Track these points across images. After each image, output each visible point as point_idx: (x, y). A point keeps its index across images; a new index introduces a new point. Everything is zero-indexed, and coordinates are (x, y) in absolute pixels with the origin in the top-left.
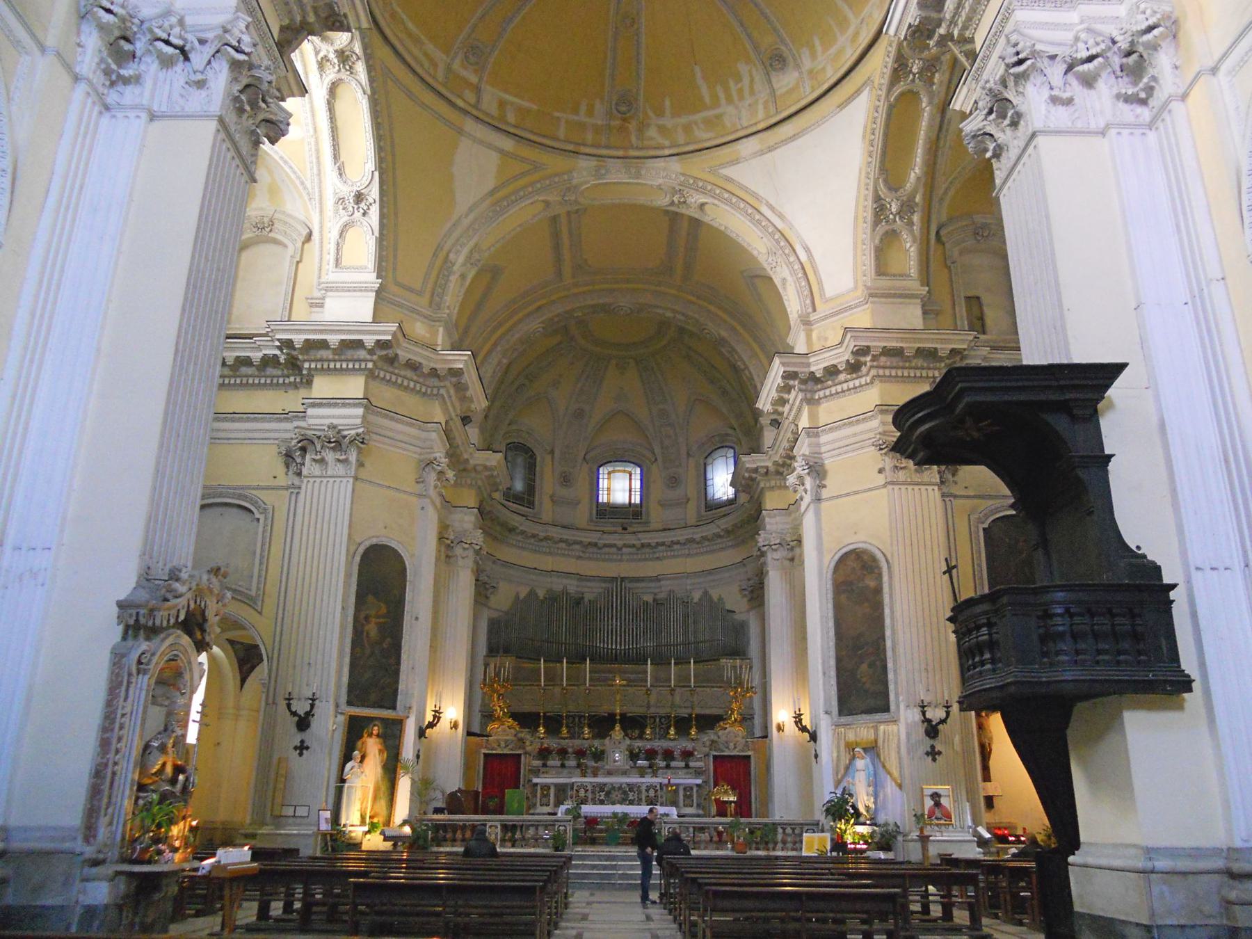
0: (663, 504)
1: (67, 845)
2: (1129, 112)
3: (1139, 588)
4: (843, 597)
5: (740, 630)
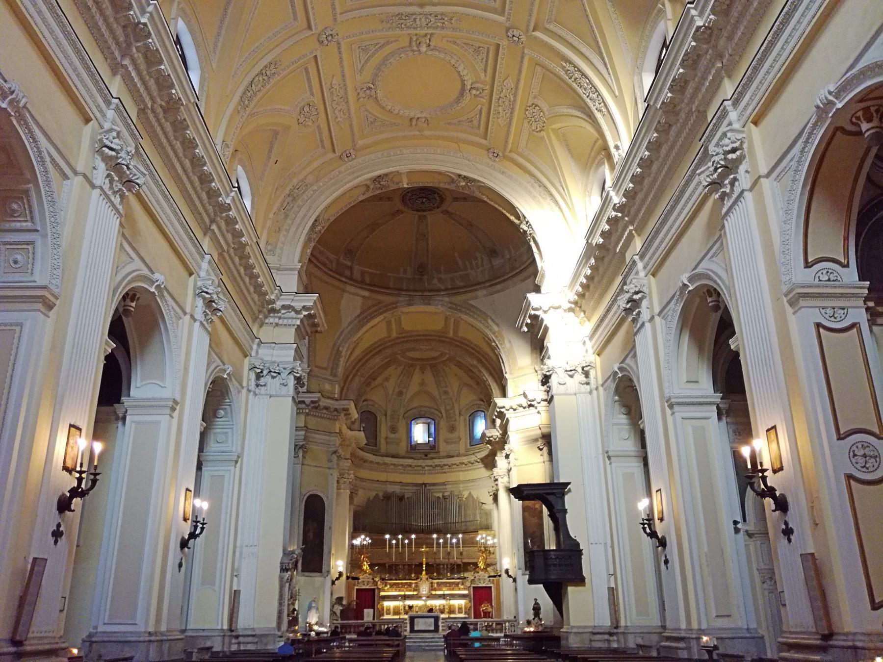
1: (272, 632)
3: (571, 551)
4: (526, 514)
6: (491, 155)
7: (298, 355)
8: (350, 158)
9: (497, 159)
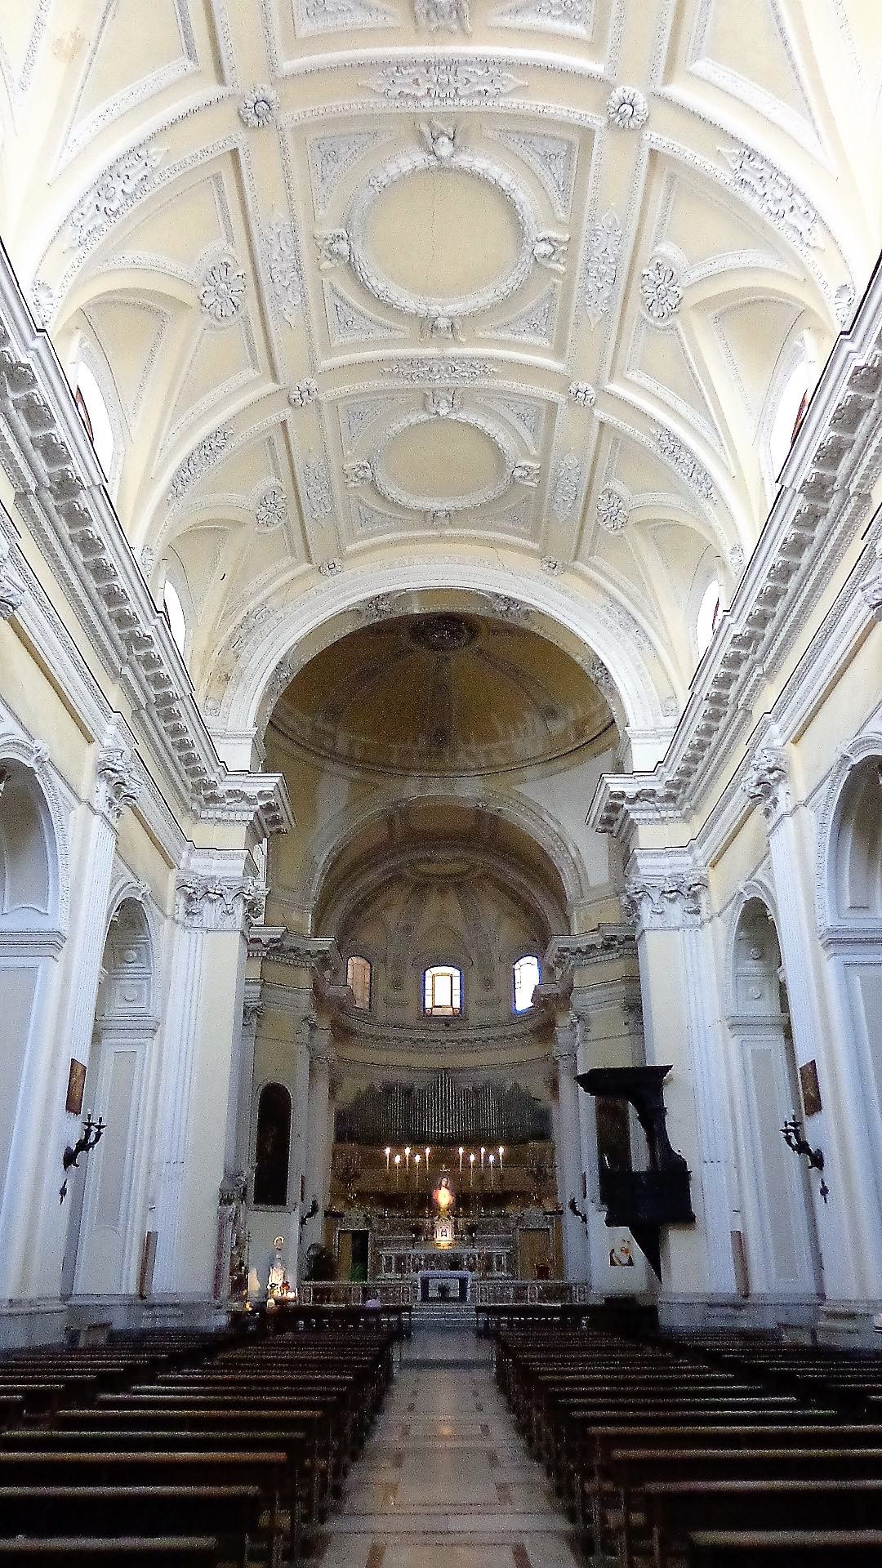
0: (481, 1003)
2: (691, 919)
5: (544, 1117)
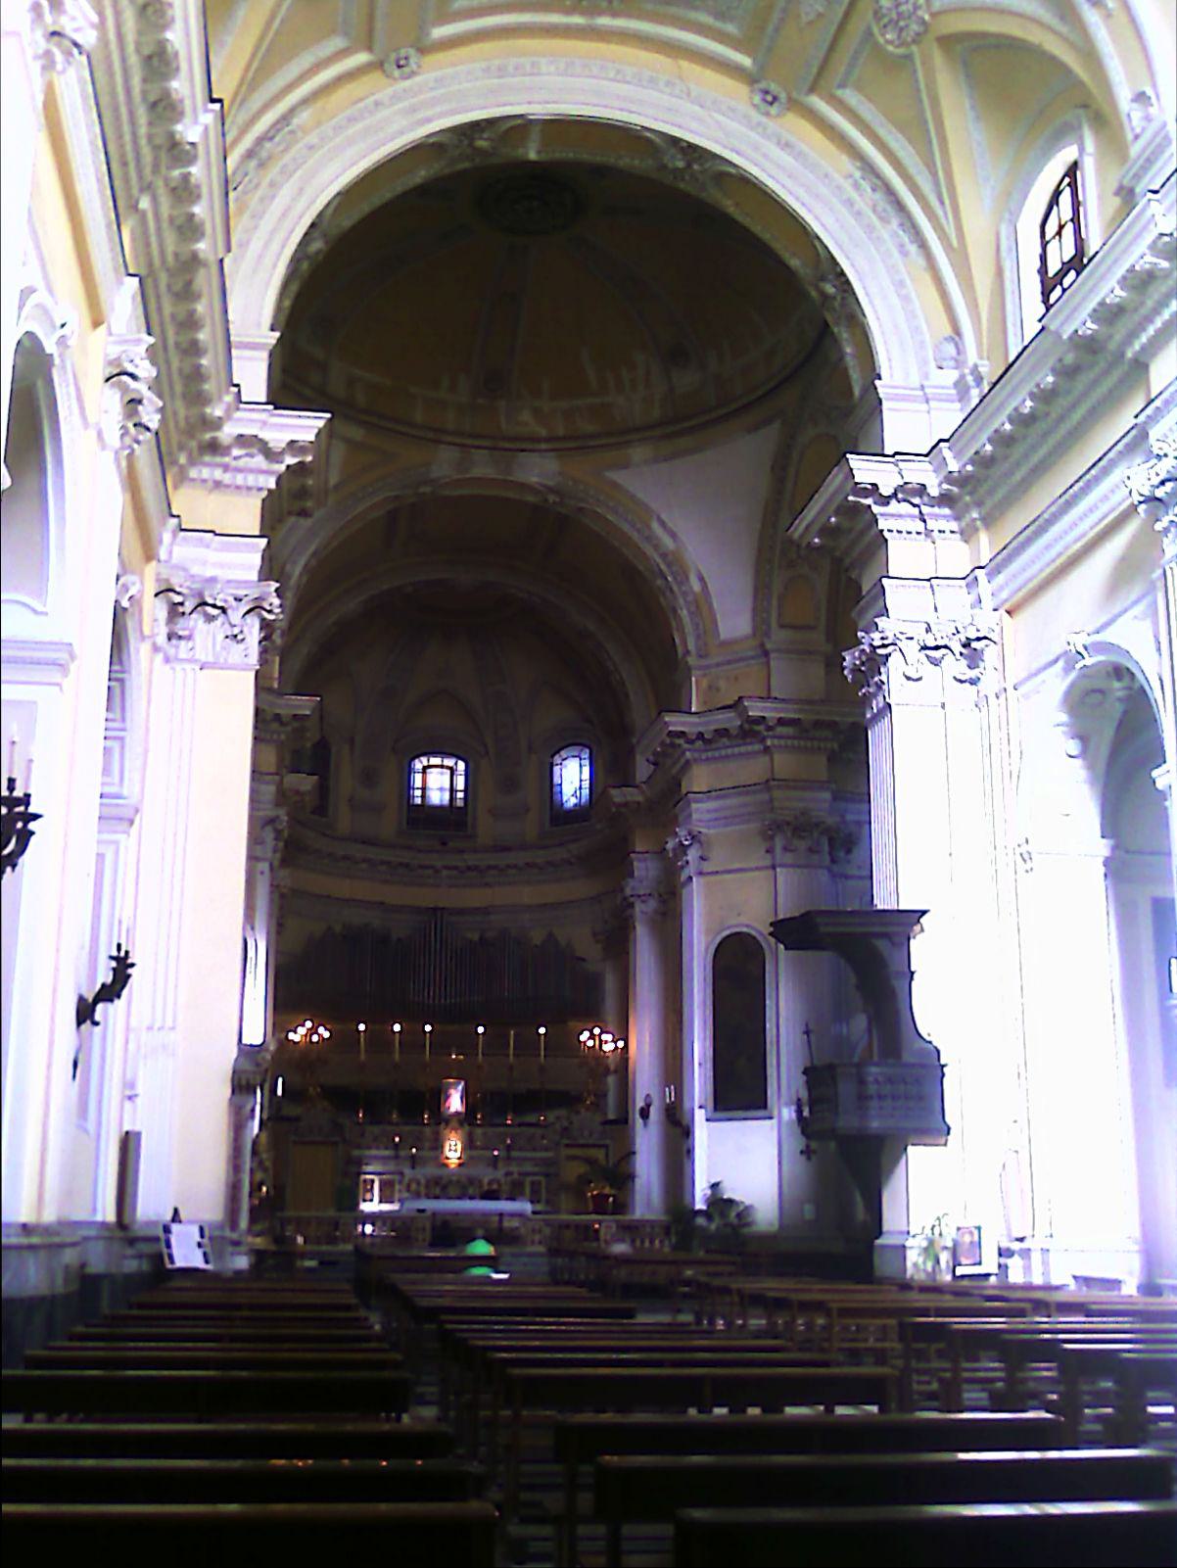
5: (594, 983)
6: (757, 99)
7: (269, 570)
8: (406, 70)
9: (773, 110)
